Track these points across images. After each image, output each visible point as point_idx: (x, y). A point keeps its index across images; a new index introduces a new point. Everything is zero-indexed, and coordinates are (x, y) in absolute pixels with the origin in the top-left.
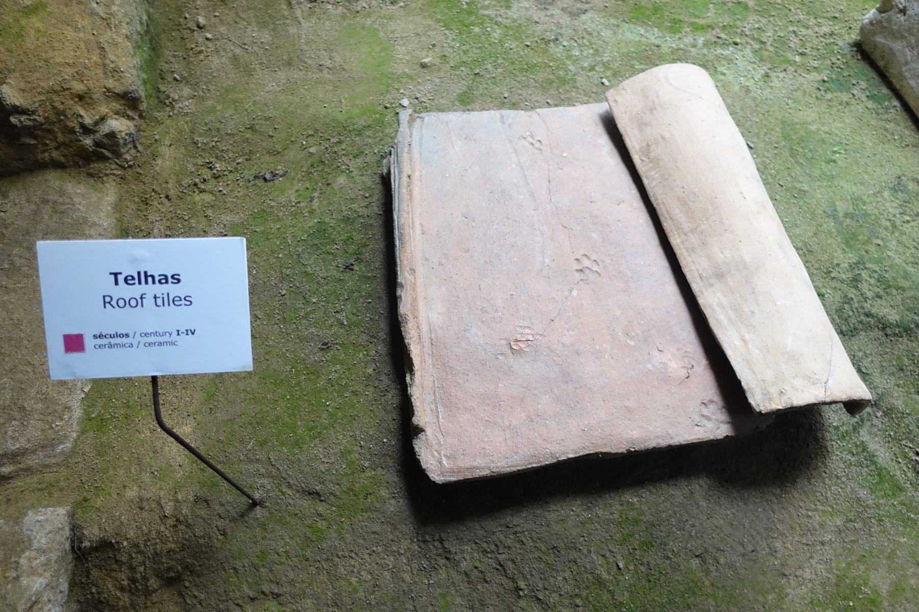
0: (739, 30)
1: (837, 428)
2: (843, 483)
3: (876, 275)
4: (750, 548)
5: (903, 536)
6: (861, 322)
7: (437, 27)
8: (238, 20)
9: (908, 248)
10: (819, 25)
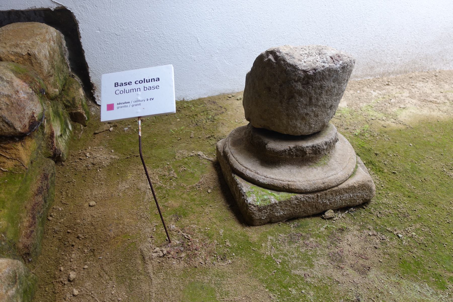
7: (262, 288)
8: (102, 273)
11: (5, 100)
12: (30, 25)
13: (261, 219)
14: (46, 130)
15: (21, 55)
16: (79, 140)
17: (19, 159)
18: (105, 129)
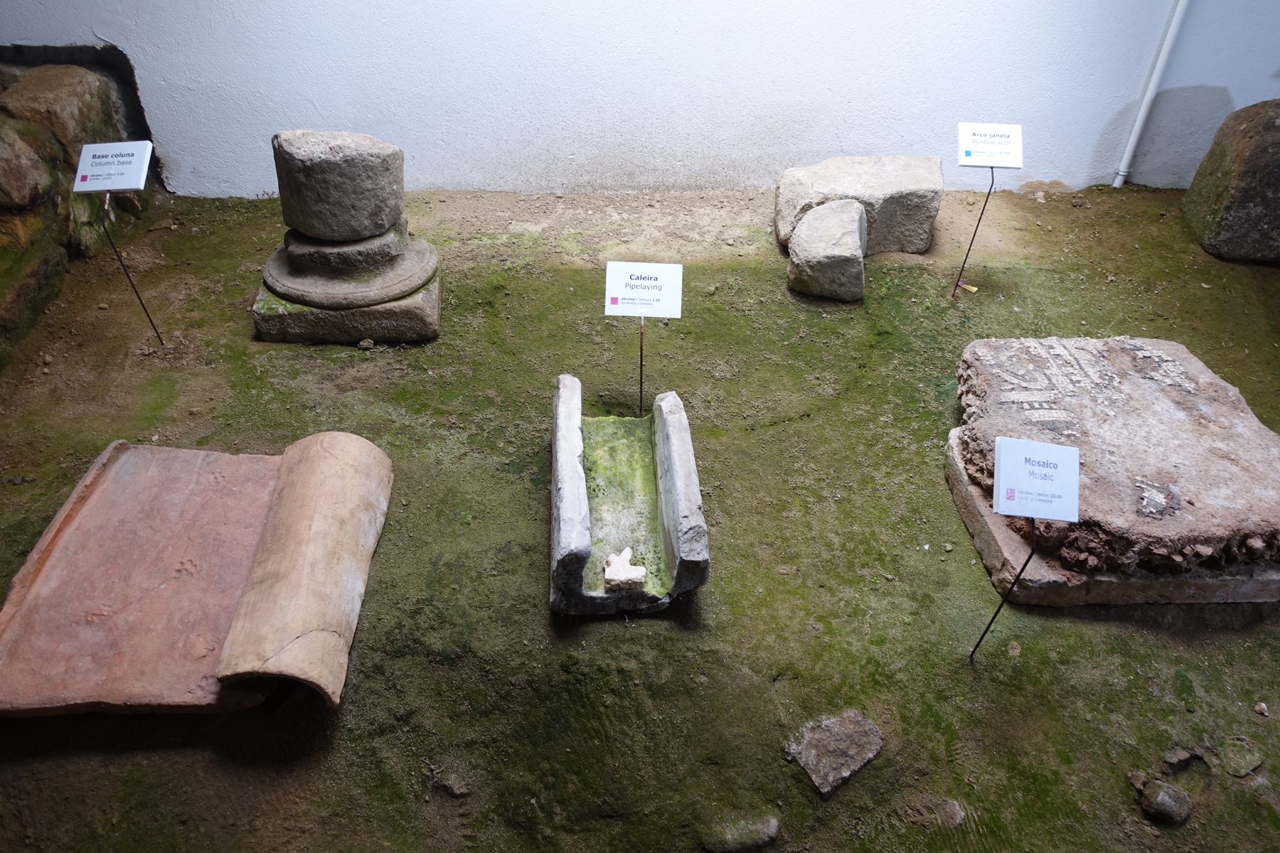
1: (350, 730)
2: (340, 779)
3: (436, 611)
4: (231, 821)
5: (387, 838)
6: (408, 646)
9: (479, 595)
11: (4, 164)
12: (63, 71)
13: (269, 333)
14: (61, 210)
15: (38, 112)
16: (123, 237)
17: (14, 235)
18: (164, 225)
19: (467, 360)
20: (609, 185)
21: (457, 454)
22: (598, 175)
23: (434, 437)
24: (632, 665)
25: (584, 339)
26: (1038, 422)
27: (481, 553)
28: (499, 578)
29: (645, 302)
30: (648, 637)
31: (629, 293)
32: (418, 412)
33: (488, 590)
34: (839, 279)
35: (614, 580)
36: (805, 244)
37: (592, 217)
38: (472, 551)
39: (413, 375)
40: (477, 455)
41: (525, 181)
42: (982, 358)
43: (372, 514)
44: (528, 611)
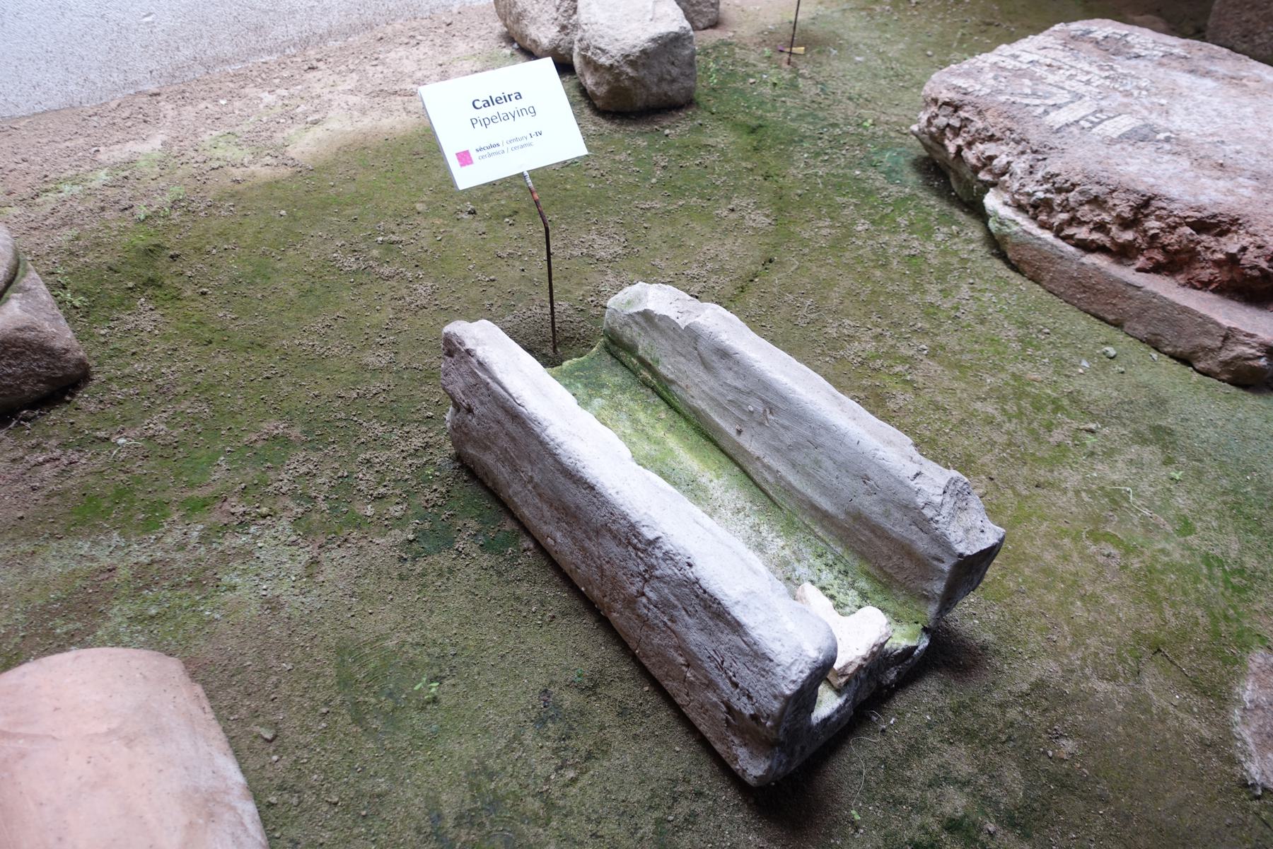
0: (270, 489)
10: (406, 437)
19: (181, 389)
20: (229, 55)
21: (299, 569)
22: (206, 41)
23: (224, 558)
24: (956, 802)
25: (364, 279)
26: (1120, 137)
27: (509, 748)
28: (585, 780)
29: (520, 143)
30: (929, 726)
31: (482, 136)
32: (149, 525)
33: (589, 820)
34: (669, 73)
35: (851, 663)
36: (611, 32)
37: (230, 108)
38: (489, 755)
39: (85, 462)
40: (342, 552)
41: (81, 81)
42: (970, 90)
43: (228, 816)
44: (694, 814)
